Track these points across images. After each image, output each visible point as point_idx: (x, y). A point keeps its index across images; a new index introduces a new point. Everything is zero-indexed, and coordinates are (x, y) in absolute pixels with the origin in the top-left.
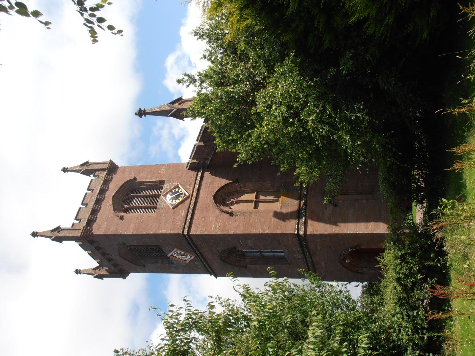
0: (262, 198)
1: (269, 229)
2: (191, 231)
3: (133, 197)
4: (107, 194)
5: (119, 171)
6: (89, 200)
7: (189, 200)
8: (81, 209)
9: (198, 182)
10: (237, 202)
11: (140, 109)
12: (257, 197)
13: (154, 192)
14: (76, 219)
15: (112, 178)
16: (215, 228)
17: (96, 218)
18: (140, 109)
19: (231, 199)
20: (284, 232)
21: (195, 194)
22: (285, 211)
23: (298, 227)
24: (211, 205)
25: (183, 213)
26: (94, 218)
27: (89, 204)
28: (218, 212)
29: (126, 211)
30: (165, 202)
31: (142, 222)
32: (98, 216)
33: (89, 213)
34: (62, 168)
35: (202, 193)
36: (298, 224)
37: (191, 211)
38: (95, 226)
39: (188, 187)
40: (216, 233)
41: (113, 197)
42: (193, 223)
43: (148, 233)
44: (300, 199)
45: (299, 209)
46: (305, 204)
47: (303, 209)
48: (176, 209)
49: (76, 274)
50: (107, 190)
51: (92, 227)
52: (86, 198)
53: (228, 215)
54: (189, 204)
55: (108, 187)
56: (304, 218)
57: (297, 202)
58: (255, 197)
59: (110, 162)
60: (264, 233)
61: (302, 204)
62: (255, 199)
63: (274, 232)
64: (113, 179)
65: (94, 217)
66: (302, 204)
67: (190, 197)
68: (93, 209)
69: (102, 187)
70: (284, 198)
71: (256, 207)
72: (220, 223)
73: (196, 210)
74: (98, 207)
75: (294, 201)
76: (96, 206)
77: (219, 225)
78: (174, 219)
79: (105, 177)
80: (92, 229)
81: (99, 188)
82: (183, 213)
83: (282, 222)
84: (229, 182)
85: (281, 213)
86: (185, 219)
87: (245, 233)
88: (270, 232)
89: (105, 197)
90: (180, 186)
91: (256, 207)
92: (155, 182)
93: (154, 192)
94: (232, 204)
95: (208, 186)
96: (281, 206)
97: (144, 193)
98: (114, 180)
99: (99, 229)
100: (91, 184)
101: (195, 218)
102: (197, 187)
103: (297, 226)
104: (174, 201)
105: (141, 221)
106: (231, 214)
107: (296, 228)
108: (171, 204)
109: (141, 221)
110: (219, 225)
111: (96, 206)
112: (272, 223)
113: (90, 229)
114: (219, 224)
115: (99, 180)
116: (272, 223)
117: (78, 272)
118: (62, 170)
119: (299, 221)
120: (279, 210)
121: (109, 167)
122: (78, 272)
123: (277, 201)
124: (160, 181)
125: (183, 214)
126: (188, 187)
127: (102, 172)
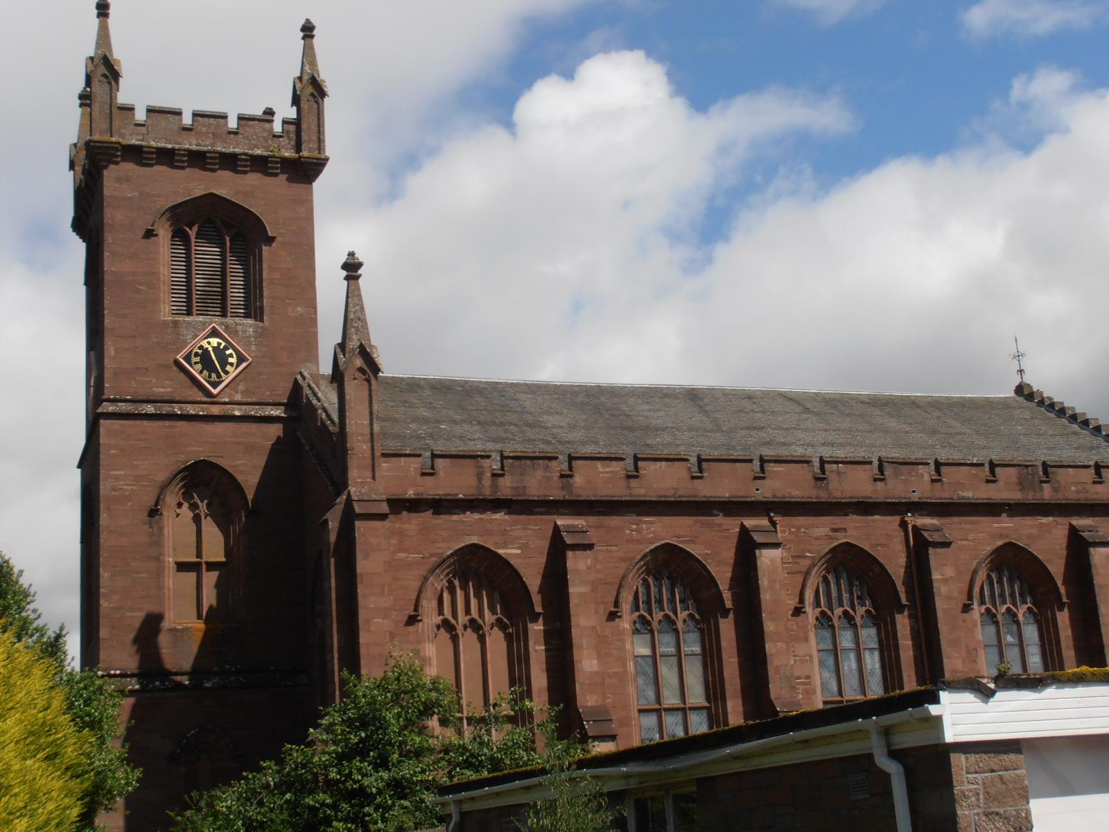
0: (210, 578)
1: (112, 609)
2: (108, 421)
3: (222, 245)
4: (226, 175)
5: (298, 188)
6: (204, 129)
7: (200, 397)
8: (177, 117)
9: (253, 411)
10: (197, 519)
11: (360, 265)
12: (211, 566)
13: (236, 293)
14: (151, 111)
15: (276, 175)
16: (117, 478)
17: (151, 165)
18: (360, 265)
19: (206, 501)
20: (103, 645)
21: (215, 410)
22: (164, 640)
23: (115, 676)
24: (182, 457)
25: (164, 390)
26: (146, 159)
27: (193, 133)
28: (162, 477)
29: (179, 235)
30: (197, 336)
31: (138, 291)
32: (157, 168)
33: (161, 145)
34: (314, 22)
35: (219, 428)
36: (122, 676)
37: (166, 409)
38: (128, 168)
39: (241, 387)
40: (101, 483)
41: (212, 195)
42: (131, 422)
43: (106, 312)
44: (195, 672)
45: (166, 674)
46: (179, 685)
47: (162, 683)
48: (175, 368)
49: (300, 26)
50: (237, 172)
51: (123, 160)
52: (212, 120)
53: (152, 503)
54: (190, 399)
55: (245, 173)
56: (137, 687)
57: (187, 665)
58: (213, 559)
59: (323, 159)
60: (101, 598)
61: (178, 678)
62: (202, 561)
63: (102, 621)
64: (271, 178)
65: (152, 159)
66: (178, 678)
67: (209, 400)
68: (173, 150)
69: (244, 157)
70: (200, 635)
71: (182, 567)
72: (129, 488)
73: (167, 423)
74: (183, 161)
75: (191, 660)
76: (184, 155)
77: (125, 487)
78: (147, 369)
79: (274, 157)
80: (117, 163)
81: (237, 150)
82: (164, 390)
83: (131, 636)
84: (250, 497)
85: (157, 631)
86: (144, 398)
87: (101, 552)
88: (102, 611)
89: (214, 171)
90: (244, 365)
91: (182, 567)
92: (261, 296)
93: (236, 293)
94: (194, 507)
95: (240, 440)
96: (176, 630)
97: (234, 267)
98: (269, 180)
99: (119, 180)
100: (256, 122)
101: (145, 423)
102: (237, 413)
103: (118, 672)
104: (198, 359)
105: (141, 287)
106: (154, 512)
107: (112, 672)
108: (191, 351)
109: (141, 287)
110: (125, 487)
111: (184, 155)
112: (129, 614)
113: (117, 156)
114: (129, 485)
115: (266, 139)
116: (129, 614)
117: (308, 30)
118: (307, 20)
119: (132, 676)
120: (166, 624)
121: (303, 160)
122: (308, 30)
123: (199, 617)
124: (262, 308)
125: (160, 391)
126: (241, 387)
127: (293, 143)
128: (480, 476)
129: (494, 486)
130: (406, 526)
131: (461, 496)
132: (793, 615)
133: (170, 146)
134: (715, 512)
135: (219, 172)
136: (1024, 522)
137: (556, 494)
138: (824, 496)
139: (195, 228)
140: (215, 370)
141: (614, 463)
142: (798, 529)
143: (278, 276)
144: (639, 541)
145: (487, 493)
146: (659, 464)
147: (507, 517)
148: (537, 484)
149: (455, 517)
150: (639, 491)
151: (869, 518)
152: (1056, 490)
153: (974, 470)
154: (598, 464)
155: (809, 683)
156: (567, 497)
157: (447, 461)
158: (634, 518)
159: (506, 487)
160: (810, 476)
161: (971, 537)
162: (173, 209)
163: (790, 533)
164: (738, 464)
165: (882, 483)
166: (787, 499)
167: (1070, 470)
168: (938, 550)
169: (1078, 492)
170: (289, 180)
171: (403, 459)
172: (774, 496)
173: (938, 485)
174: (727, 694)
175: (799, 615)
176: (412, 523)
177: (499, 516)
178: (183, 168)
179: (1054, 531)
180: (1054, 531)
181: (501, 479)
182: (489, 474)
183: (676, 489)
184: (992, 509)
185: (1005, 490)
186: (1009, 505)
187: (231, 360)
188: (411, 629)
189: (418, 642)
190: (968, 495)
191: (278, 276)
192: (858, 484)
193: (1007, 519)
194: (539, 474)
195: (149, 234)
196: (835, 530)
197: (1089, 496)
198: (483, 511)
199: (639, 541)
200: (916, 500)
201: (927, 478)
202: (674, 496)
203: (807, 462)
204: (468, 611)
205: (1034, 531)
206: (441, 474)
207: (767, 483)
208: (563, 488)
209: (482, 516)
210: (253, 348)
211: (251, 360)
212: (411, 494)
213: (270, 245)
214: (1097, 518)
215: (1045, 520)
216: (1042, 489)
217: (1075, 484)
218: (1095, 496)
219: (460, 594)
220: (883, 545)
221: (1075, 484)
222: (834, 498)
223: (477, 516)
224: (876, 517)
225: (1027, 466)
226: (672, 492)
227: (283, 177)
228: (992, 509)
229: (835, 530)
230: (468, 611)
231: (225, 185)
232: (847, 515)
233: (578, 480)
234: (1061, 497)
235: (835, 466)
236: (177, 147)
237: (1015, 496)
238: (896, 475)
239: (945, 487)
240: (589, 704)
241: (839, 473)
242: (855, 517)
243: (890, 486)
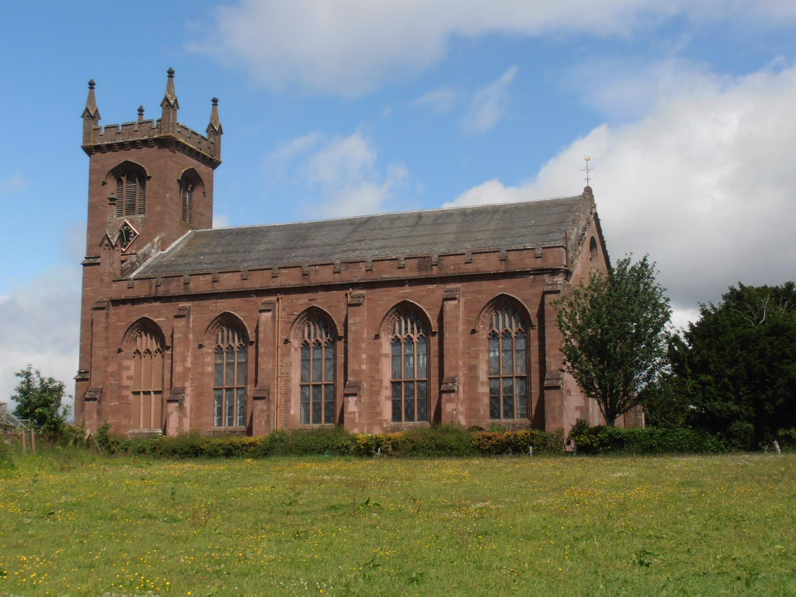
4: (134, 150)
17: (106, 152)
32: (108, 153)
52: (128, 127)
80: (94, 154)
115: (149, 131)
128: (151, 287)
129: (156, 291)
130: (121, 311)
131: (142, 296)
132: (284, 343)
133: (110, 143)
134: (252, 295)
135: (132, 150)
136: (418, 289)
137: (182, 293)
138: (306, 284)
139: (125, 176)
140: (124, 241)
141: (208, 276)
142: (292, 301)
143: (151, 194)
144: (215, 312)
145: (153, 294)
146: (227, 274)
147: (160, 304)
148: (174, 288)
149: (139, 306)
150: (219, 288)
151: (330, 293)
152: (440, 269)
153: (392, 263)
154: (201, 277)
155: (288, 376)
156: (186, 294)
157: (139, 281)
158: (215, 301)
159: (161, 292)
160: (300, 274)
161: (385, 298)
162: (112, 170)
163: (288, 303)
164: (265, 271)
165: (339, 274)
166: (288, 286)
167: (452, 257)
168: (353, 308)
169: (454, 269)
170: (159, 148)
171: (121, 282)
172: (281, 285)
173: (369, 272)
174: (248, 381)
175: (474, 334)
176: (123, 309)
177: (157, 304)
178: (117, 151)
179: (436, 292)
180: (436, 292)
181: (159, 287)
182: (154, 286)
183: (235, 286)
184: (400, 283)
185: (410, 273)
186: (408, 280)
187: (131, 235)
188: (119, 354)
189: (121, 360)
190: (387, 276)
191: (151, 194)
192: (325, 276)
193: (409, 288)
194: (175, 284)
195: (104, 183)
196: (311, 300)
197: (462, 271)
198: (151, 302)
199: (215, 312)
200: (357, 281)
201: (364, 269)
202: (233, 289)
203: (300, 267)
204: (504, 325)
205: (423, 293)
206: (136, 287)
207: (279, 279)
208: (184, 289)
209: (151, 304)
210: (141, 228)
211: (138, 234)
212: (123, 297)
213: (149, 180)
214: (465, 284)
215: (431, 287)
216: (432, 269)
217: (453, 265)
218: (465, 271)
219: (312, 327)
220: (335, 306)
221: (453, 265)
222: (312, 284)
223: (148, 304)
224: (334, 292)
225: (425, 257)
226: (232, 287)
227: (156, 147)
228: (400, 283)
229: (311, 300)
230: (504, 325)
231: (132, 156)
232: (317, 292)
233: (191, 285)
234: (443, 273)
235: (314, 267)
236: (113, 142)
237: (415, 274)
238: (346, 269)
239: (374, 273)
240: (177, 386)
241: (316, 271)
242: (322, 293)
243: (342, 276)
